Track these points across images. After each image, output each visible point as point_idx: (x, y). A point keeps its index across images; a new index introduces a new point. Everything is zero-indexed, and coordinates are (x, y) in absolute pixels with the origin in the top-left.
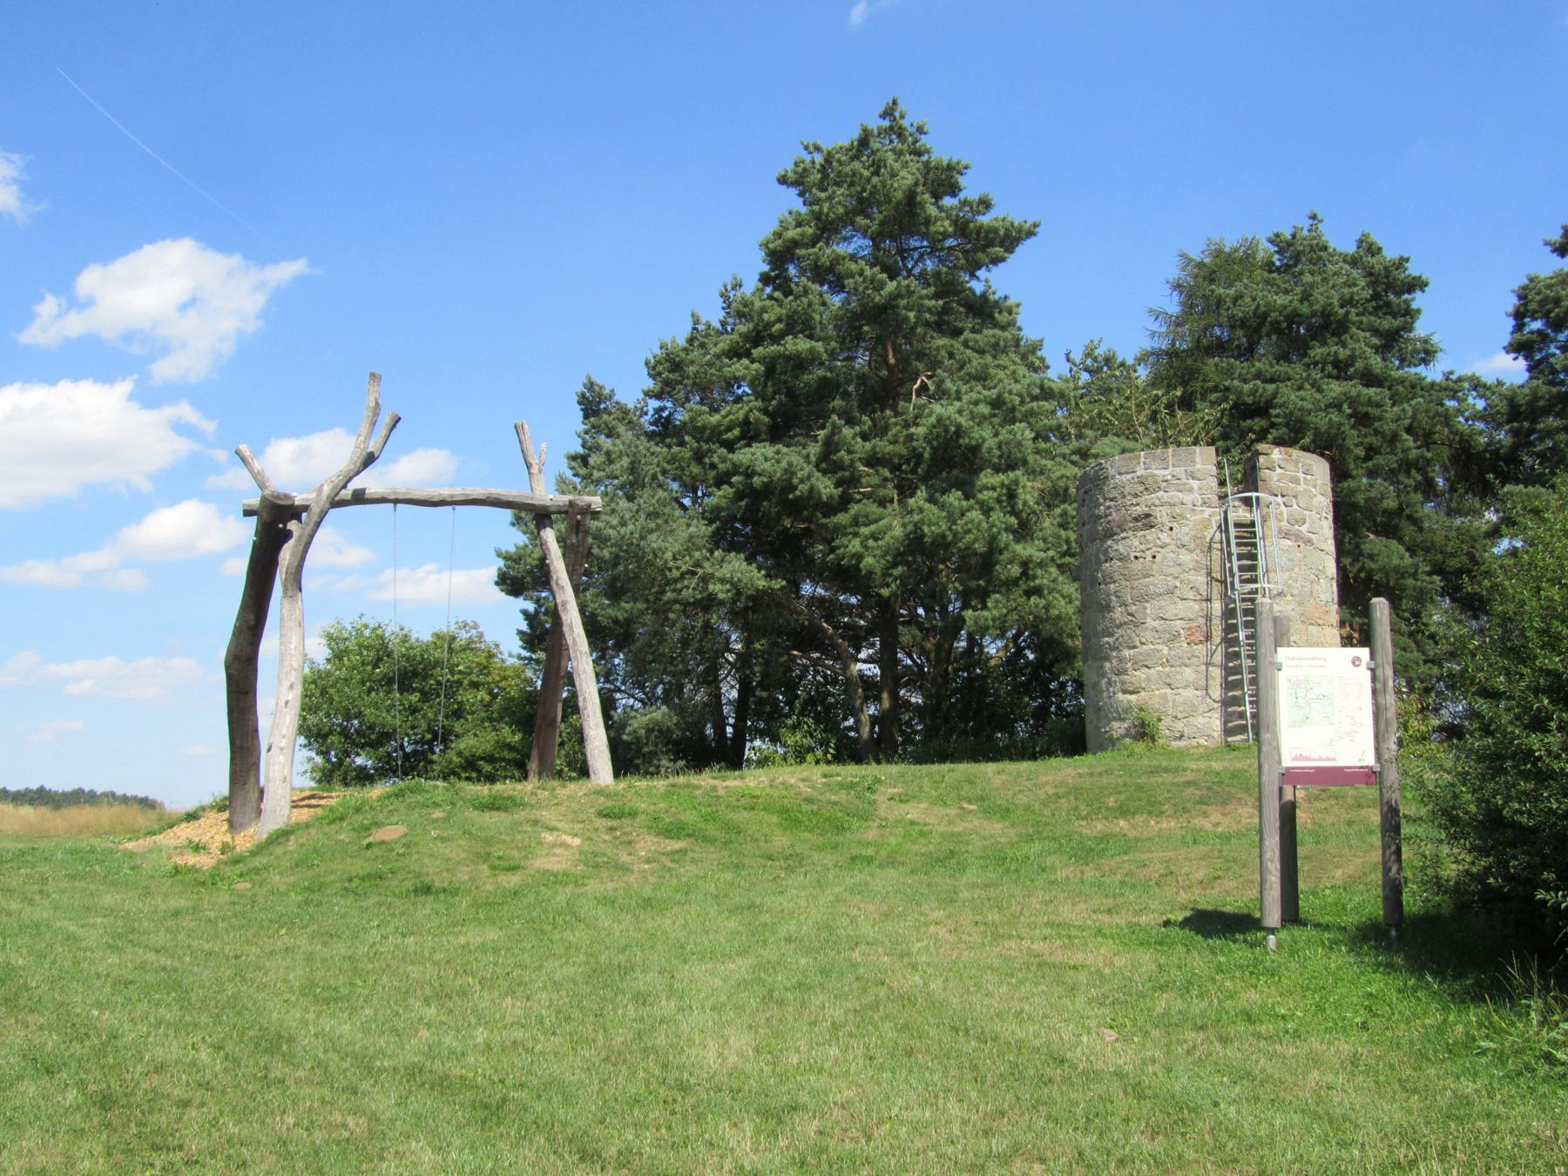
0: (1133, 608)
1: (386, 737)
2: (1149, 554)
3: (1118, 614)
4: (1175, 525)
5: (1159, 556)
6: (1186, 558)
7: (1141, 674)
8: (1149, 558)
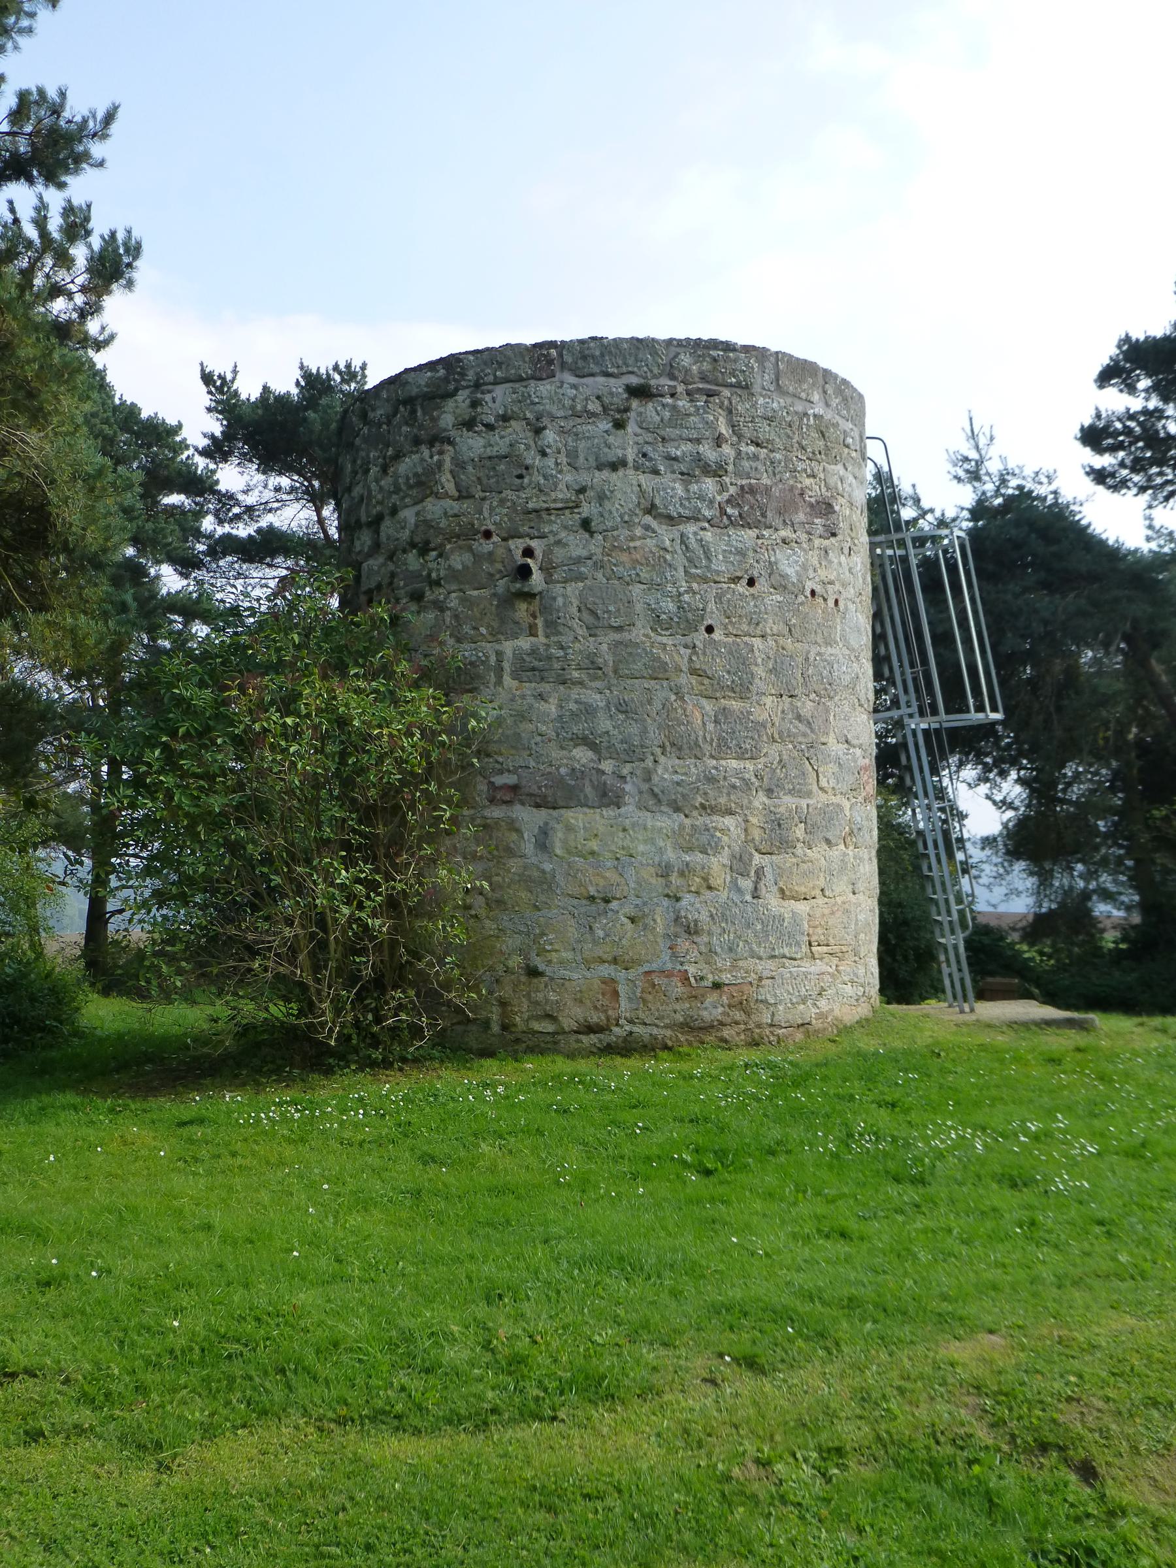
0: (807, 707)
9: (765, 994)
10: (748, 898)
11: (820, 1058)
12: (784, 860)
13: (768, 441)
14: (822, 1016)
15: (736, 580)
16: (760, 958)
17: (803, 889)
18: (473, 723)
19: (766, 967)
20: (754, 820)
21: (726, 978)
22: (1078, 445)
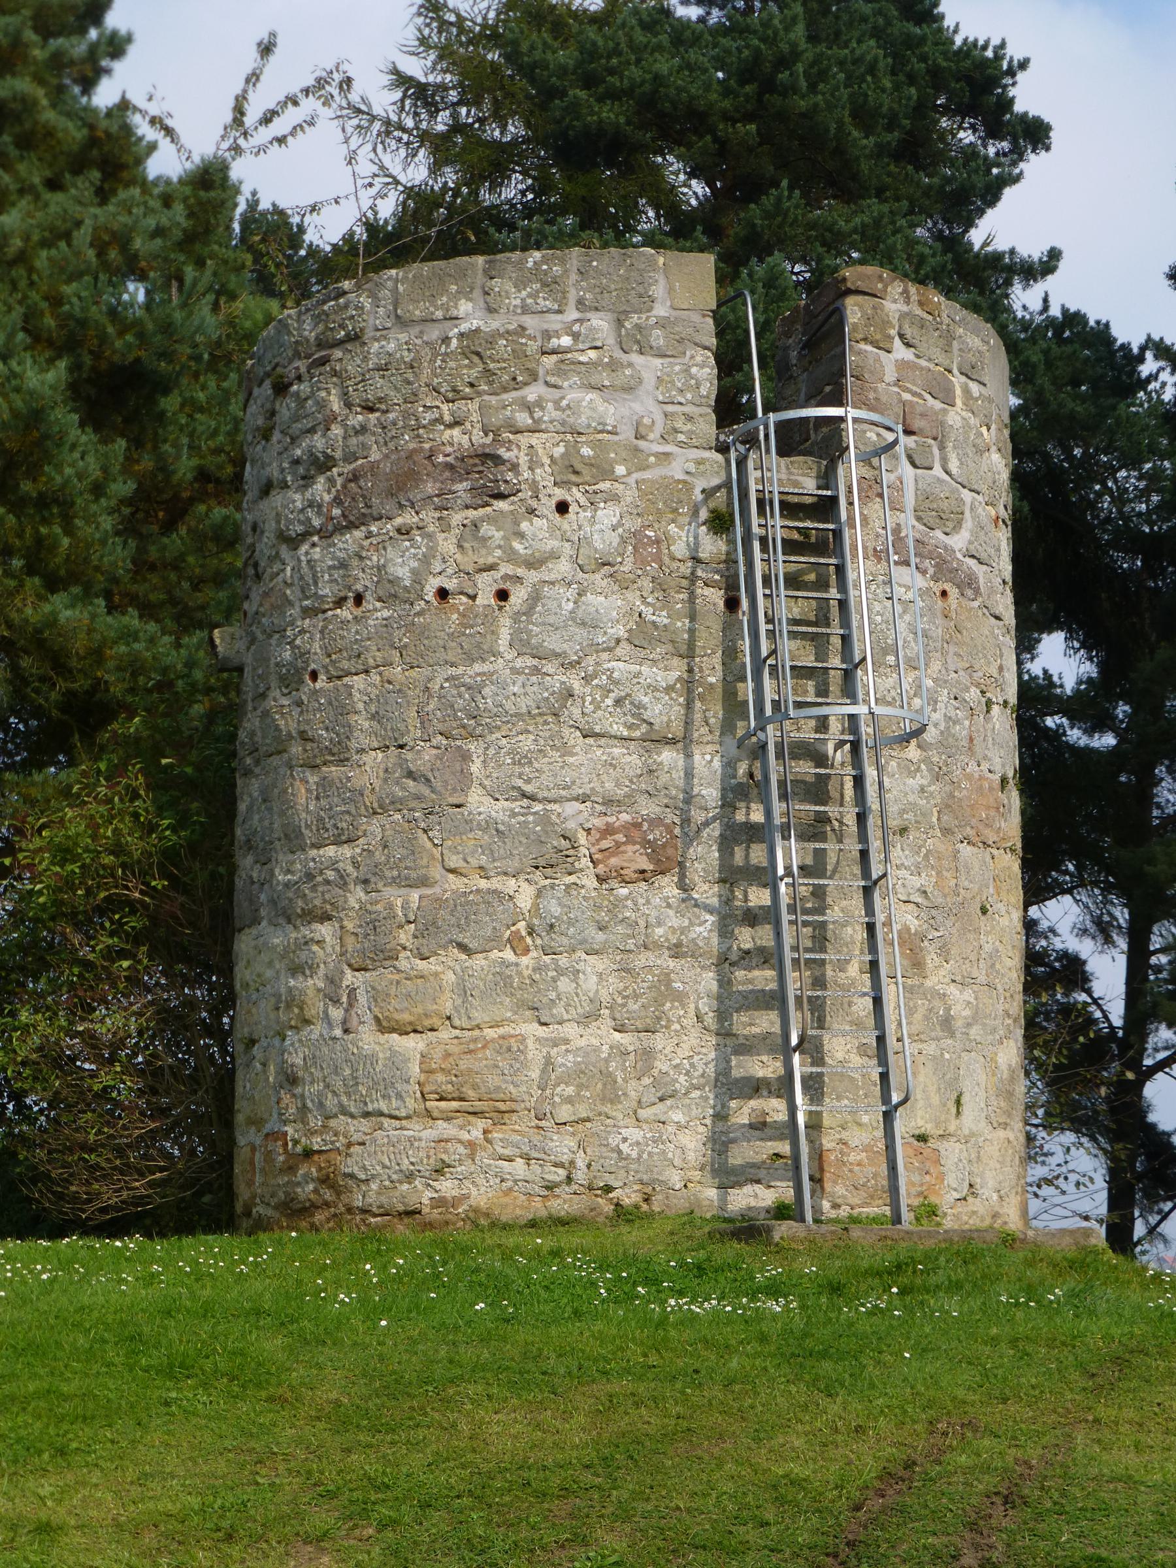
0: (424, 757)
1: (944, 267)
2: (486, 586)
3: (370, 768)
4: (574, 495)
5: (518, 596)
6: (608, 605)
7: (445, 967)
8: (486, 598)
9: (351, 1166)
10: (338, 1032)
11: (1120, 1470)
12: (382, 977)
13: (381, 400)
14: (440, 1202)
15: (340, 602)
16: (352, 1116)
17: (406, 1017)
18: (995, 171)
19: (358, 1128)
20: (349, 925)
21: (316, 1143)
22: (1046, 118)
